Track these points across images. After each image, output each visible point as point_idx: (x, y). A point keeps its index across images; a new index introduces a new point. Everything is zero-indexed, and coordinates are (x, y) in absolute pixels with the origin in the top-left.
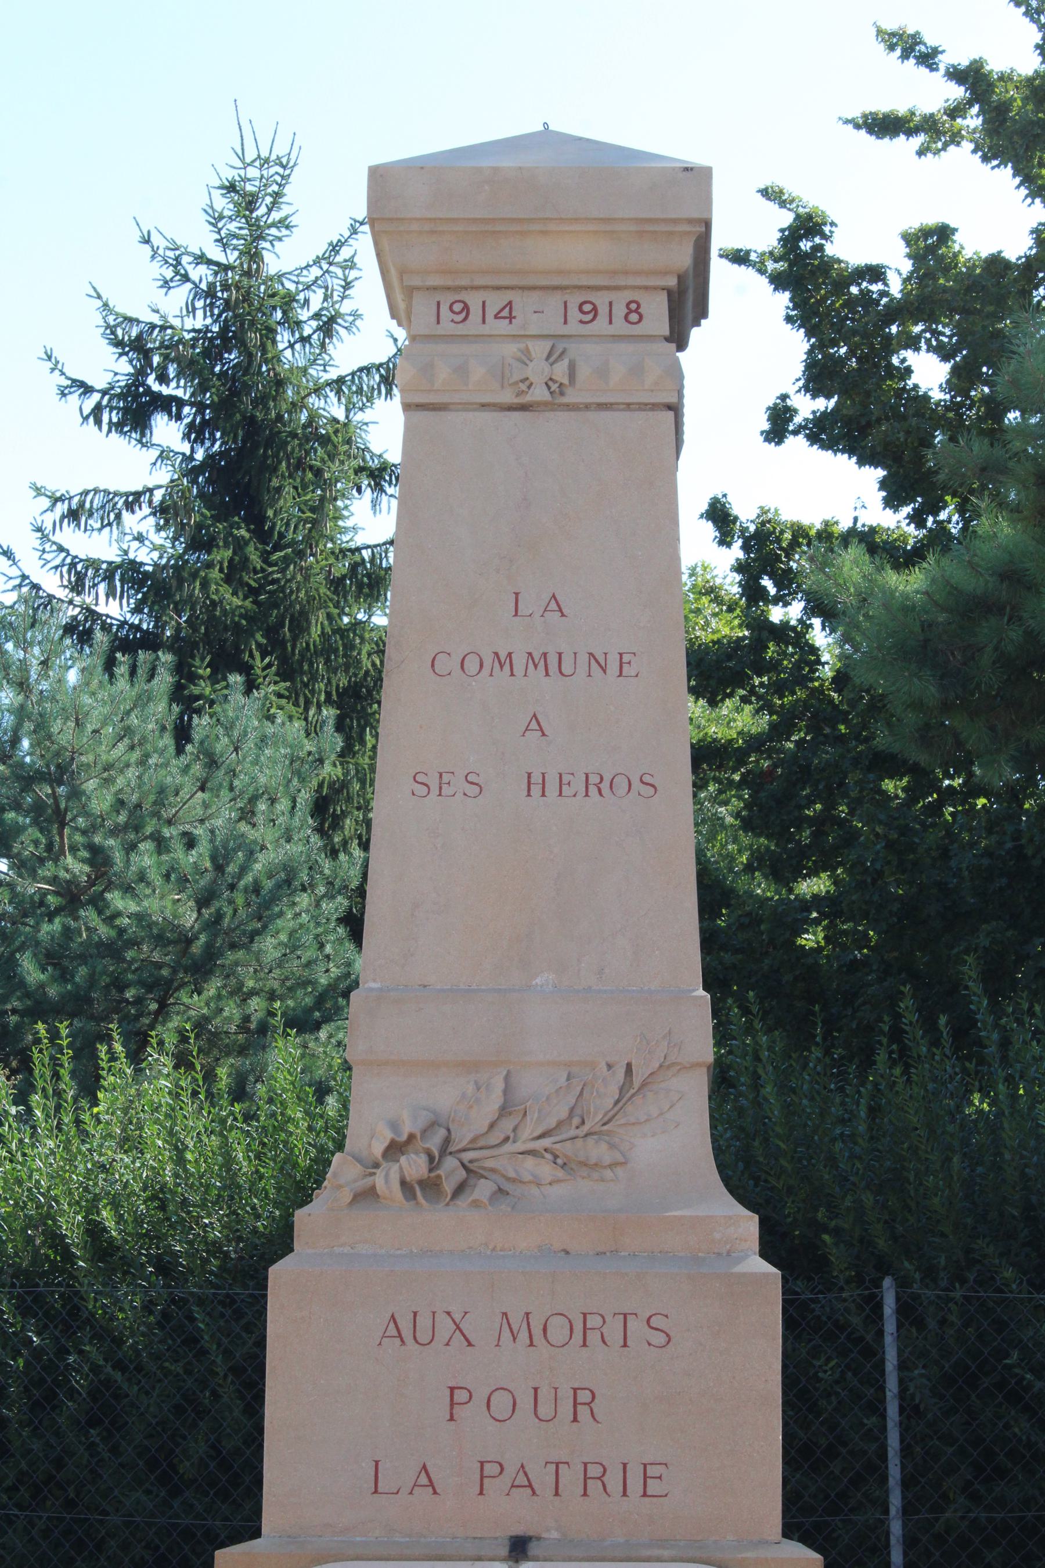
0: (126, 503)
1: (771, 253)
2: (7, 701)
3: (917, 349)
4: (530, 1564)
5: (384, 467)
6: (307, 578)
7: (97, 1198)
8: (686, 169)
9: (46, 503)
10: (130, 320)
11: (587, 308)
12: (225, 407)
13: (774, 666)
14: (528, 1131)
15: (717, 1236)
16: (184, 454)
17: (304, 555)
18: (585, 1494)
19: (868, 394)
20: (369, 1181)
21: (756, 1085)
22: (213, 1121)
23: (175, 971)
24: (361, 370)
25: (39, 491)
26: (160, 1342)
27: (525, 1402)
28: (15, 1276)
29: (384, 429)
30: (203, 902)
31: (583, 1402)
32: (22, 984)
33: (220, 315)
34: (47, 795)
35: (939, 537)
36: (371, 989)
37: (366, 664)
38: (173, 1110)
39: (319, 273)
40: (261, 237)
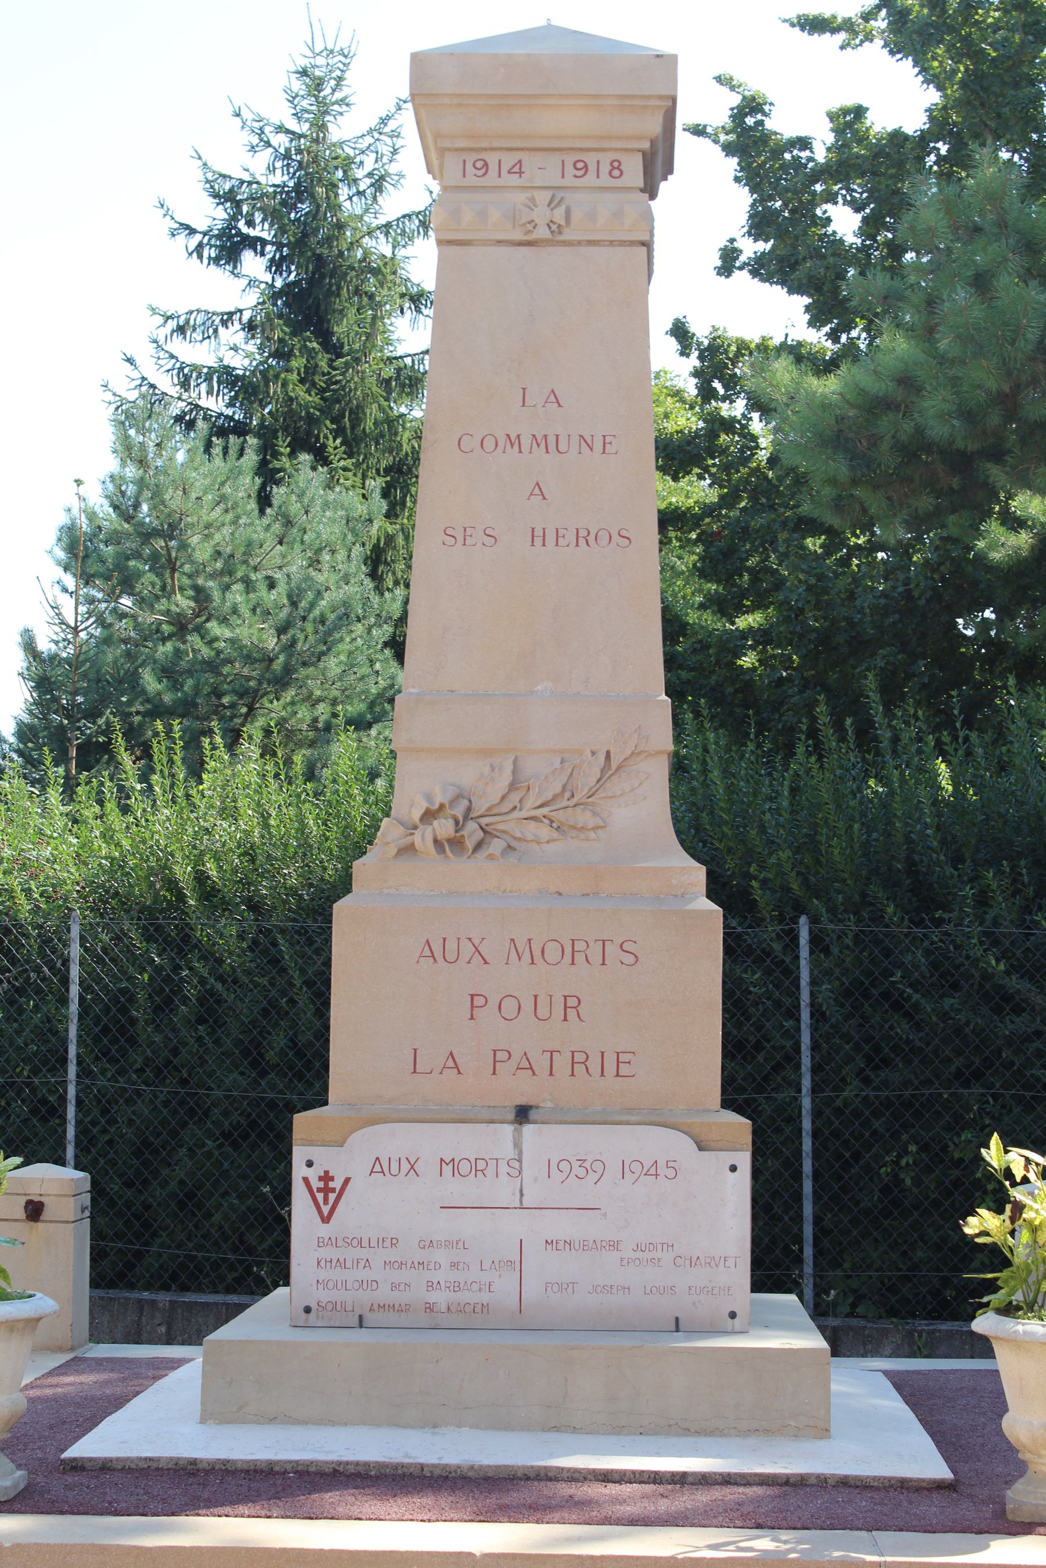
0: (222, 320)
1: (723, 127)
2: (131, 475)
3: (836, 203)
4: (531, 1126)
5: (421, 294)
6: (363, 379)
7: (202, 853)
8: (658, 56)
9: (160, 320)
10: (224, 176)
11: (580, 165)
12: (300, 244)
13: (724, 451)
14: (531, 801)
15: (675, 882)
16: (267, 283)
17: (360, 361)
18: (573, 1075)
19: (797, 238)
20: (409, 839)
21: (705, 771)
22: (290, 796)
23: (260, 683)
24: (404, 217)
25: (154, 311)
26: (251, 961)
27: (528, 1006)
28: (141, 912)
29: (421, 263)
30: (281, 631)
31: (571, 1006)
32: (144, 692)
33: (294, 174)
34: (161, 547)
35: (850, 351)
36: (412, 694)
37: (406, 448)
38: (260, 787)
39: (372, 141)
40: (326, 112)
